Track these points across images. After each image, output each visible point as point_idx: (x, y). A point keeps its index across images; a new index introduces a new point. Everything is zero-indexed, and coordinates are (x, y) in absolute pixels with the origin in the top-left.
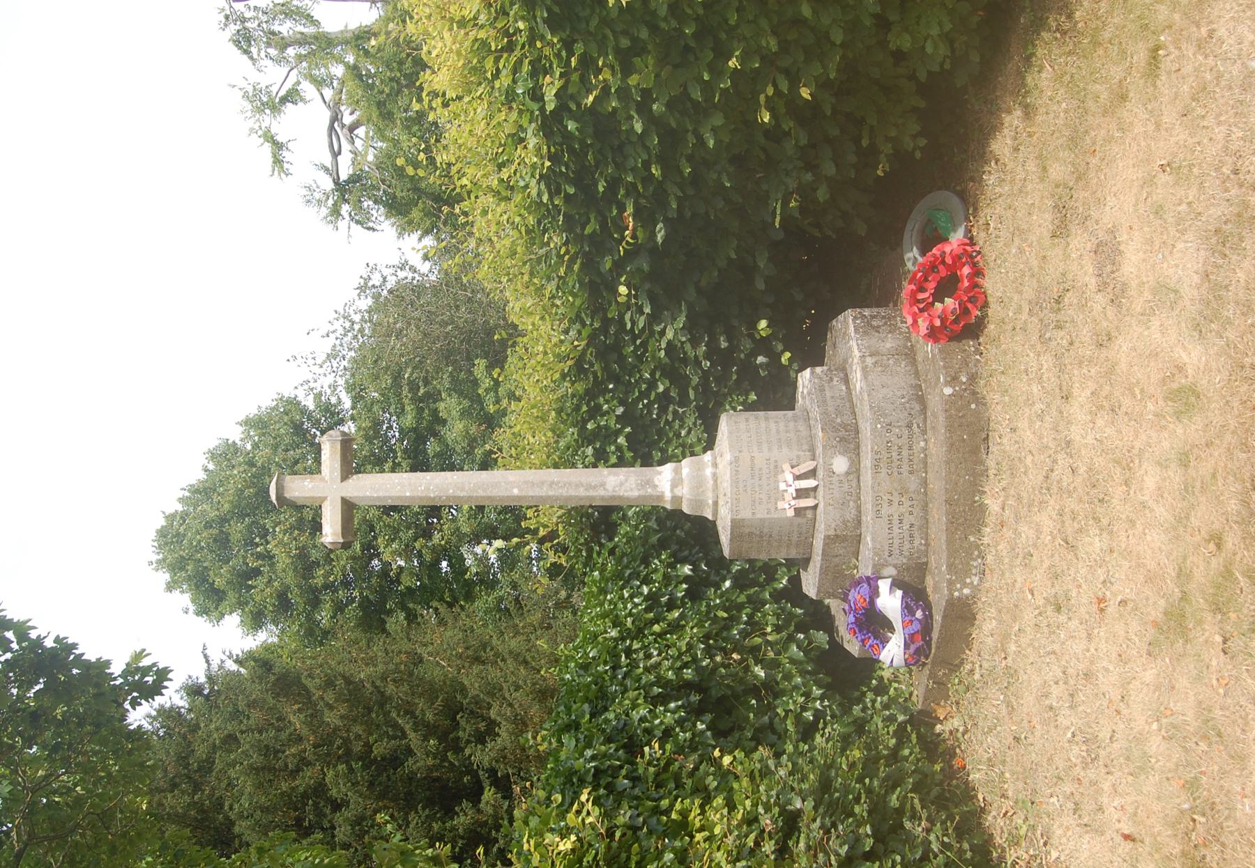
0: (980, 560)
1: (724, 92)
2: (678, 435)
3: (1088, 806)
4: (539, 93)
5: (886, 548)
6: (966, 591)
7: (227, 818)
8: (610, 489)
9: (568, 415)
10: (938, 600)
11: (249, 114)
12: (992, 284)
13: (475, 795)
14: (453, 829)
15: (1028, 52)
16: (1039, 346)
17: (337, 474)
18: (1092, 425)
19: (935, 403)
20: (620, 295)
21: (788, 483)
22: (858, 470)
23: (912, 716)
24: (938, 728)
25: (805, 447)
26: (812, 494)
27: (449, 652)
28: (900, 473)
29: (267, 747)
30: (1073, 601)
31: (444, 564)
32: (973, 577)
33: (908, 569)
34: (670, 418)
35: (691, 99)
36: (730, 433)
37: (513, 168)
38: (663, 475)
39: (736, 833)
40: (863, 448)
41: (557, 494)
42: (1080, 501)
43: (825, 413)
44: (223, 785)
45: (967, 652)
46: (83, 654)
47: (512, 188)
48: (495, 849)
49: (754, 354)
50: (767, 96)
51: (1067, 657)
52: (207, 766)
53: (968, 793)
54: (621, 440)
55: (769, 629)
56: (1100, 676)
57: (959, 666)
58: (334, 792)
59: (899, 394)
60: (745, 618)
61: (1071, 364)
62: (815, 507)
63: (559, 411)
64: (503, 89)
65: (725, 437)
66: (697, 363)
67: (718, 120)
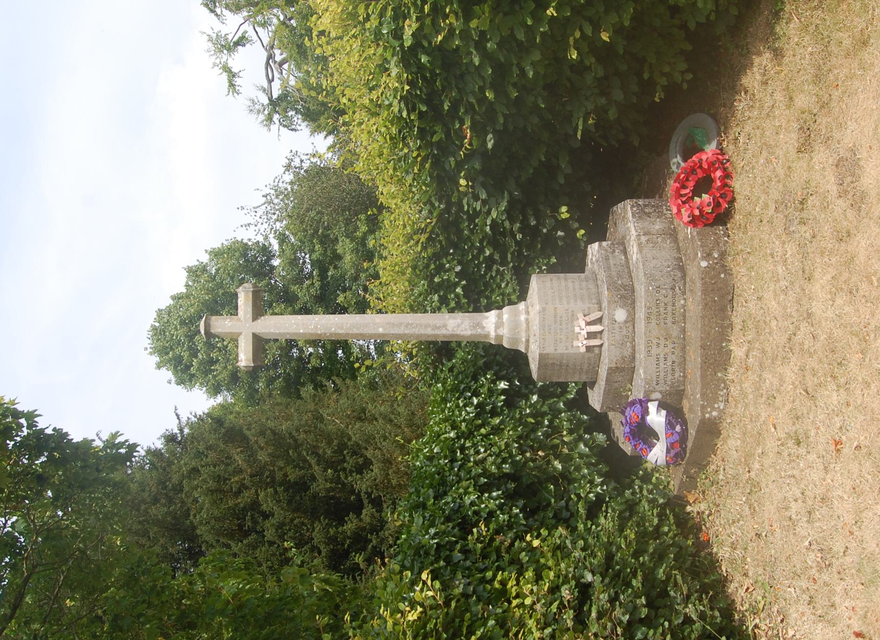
0: (725, 391)
1: (543, 34)
2: (500, 287)
3: (821, 601)
4: (399, 33)
5: (655, 379)
6: (715, 414)
7: (191, 522)
8: (450, 329)
9: (420, 271)
10: (693, 419)
11: (213, 52)
12: (738, 184)
13: (358, 508)
14: (344, 532)
15: (778, 8)
16: (784, 237)
17: (250, 316)
18: (831, 303)
19: (693, 272)
20: (461, 186)
21: (582, 328)
22: (633, 319)
23: (669, 499)
24: (689, 509)
25: (594, 301)
26: (599, 335)
27: (341, 413)
28: (665, 323)
29: (219, 476)
30: (811, 439)
31: (340, 352)
32: (720, 403)
33: (670, 394)
34: (494, 274)
35: (516, 40)
36: (539, 289)
37: (380, 91)
38: (489, 319)
39: (543, 601)
40: (638, 304)
41: (411, 332)
42: (820, 361)
43: (610, 276)
44: (190, 500)
45: (712, 456)
46: (72, 439)
47: (380, 106)
48: (370, 546)
49: (555, 229)
50: (575, 39)
51: (806, 482)
52: (178, 489)
53: (713, 563)
54: (459, 290)
55: (565, 433)
56: (836, 502)
57: (706, 466)
58: (264, 507)
59: (665, 264)
60: (546, 422)
61: (813, 253)
62: (601, 346)
63: (414, 268)
64: (372, 30)
65: (535, 293)
66: (513, 236)
67: (536, 56)
